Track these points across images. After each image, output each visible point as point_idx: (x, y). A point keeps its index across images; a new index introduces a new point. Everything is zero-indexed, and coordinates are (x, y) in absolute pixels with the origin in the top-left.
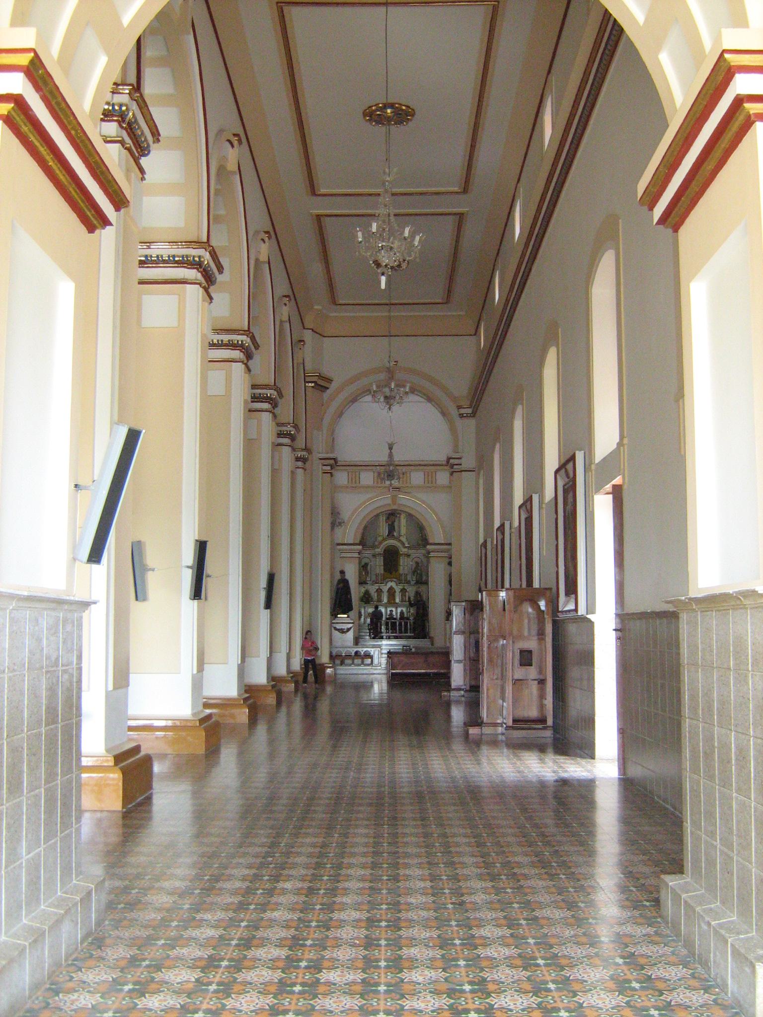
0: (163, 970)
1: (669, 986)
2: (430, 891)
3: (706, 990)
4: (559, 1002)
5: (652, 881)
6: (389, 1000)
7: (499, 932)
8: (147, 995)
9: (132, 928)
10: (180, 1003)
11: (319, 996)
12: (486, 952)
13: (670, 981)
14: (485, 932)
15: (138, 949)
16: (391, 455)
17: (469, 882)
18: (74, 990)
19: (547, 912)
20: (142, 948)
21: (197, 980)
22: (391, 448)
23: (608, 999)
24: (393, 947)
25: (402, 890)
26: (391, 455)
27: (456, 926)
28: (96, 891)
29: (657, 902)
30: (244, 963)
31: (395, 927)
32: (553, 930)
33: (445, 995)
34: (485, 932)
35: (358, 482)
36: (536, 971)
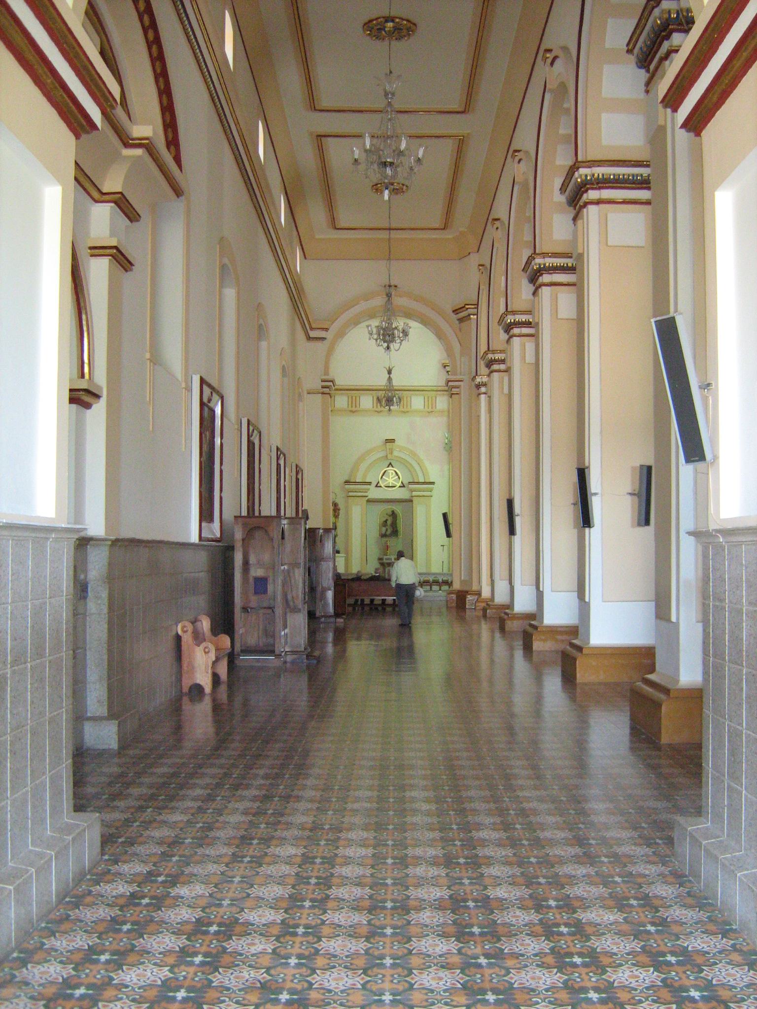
0: (163, 909)
1: (708, 960)
2: (437, 826)
3: (725, 934)
4: (572, 947)
5: (664, 816)
6: (395, 943)
7: (495, 835)
8: (125, 968)
9: (132, 863)
10: (179, 946)
11: (318, 971)
12: (511, 945)
13: (709, 953)
14: (483, 834)
15: (138, 886)
16: (390, 379)
17: (481, 832)
18: (145, 843)
19: (569, 869)
20: (143, 885)
21: (233, 854)
22: (390, 372)
23: (623, 944)
24: (399, 866)
25: (410, 879)
26: (390, 379)
27: (471, 884)
28: (56, 858)
29: (670, 841)
30: (207, 995)
31: (403, 909)
32: (539, 819)
33: (454, 939)
34: (483, 834)
35: (358, 405)
36: (547, 913)
